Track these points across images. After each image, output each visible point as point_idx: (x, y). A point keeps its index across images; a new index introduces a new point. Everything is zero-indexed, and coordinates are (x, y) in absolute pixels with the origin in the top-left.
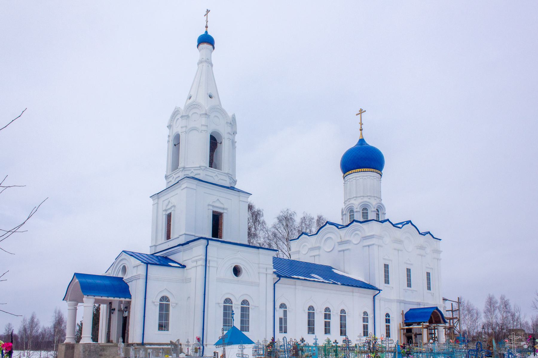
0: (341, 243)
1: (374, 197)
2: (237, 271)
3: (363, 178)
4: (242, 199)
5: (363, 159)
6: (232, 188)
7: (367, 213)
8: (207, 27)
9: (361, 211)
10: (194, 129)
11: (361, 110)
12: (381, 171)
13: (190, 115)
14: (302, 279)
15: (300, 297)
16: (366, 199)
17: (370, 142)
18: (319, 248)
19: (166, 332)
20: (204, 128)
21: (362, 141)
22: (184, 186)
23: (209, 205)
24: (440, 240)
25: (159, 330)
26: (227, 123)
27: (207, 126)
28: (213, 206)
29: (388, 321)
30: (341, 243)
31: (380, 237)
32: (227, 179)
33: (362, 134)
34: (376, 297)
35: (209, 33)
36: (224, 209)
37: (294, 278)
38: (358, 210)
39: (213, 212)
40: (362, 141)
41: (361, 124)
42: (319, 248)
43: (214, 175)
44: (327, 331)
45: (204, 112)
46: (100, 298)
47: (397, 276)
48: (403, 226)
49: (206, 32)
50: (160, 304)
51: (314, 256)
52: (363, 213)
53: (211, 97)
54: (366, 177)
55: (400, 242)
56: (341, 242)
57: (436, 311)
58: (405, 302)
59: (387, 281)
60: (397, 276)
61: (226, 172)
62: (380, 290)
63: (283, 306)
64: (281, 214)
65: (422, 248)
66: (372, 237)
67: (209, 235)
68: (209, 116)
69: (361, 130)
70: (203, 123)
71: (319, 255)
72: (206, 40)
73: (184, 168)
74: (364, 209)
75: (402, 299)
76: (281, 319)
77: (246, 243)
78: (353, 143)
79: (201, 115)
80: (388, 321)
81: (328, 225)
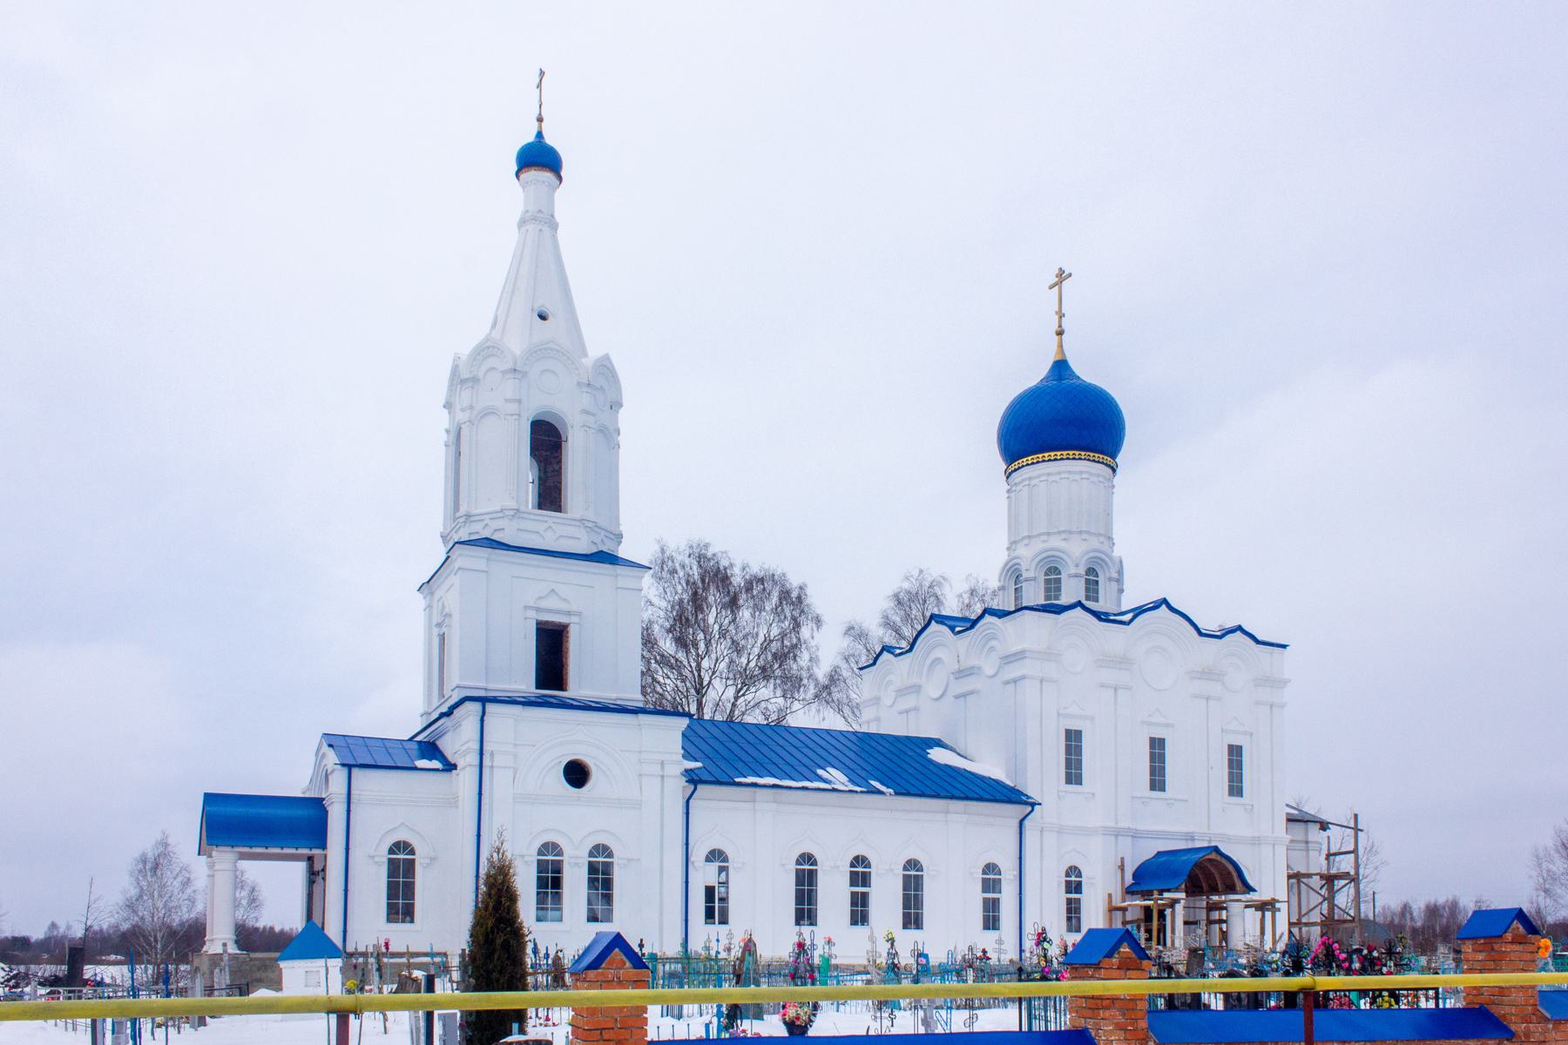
0: (961, 674)
1: (1081, 532)
2: (577, 774)
3: (1062, 477)
4: (622, 582)
5: (1064, 422)
6: (605, 558)
7: (1058, 581)
8: (540, 120)
9: (1042, 578)
10: (489, 412)
11: (1061, 271)
12: (1113, 456)
13: (481, 375)
14: (764, 786)
15: (764, 833)
16: (1055, 542)
17: (1086, 371)
18: (916, 689)
19: (407, 926)
20: (513, 408)
21: (1061, 367)
22: (457, 565)
23: (526, 608)
24: (1284, 646)
25: (389, 920)
26: (579, 384)
27: (519, 401)
28: (538, 610)
29: (1074, 887)
30: (961, 674)
31: (1048, 655)
32: (581, 533)
33: (1061, 346)
34: (1026, 822)
35: (549, 140)
36: (569, 613)
37: (740, 784)
38: (1031, 574)
39: (539, 623)
40: (1061, 367)
41: (1061, 316)
42: (916, 689)
43: (541, 527)
44: (859, 912)
45: (509, 365)
46: (246, 850)
47: (1114, 761)
48: (1134, 617)
49: (540, 135)
50: (390, 860)
51: (907, 711)
52: (1047, 582)
53: (543, 317)
54: (1057, 478)
55: (1123, 662)
56: (960, 671)
57: (1213, 856)
58: (1136, 835)
59: (1073, 775)
60: (1114, 761)
61: (578, 516)
62: (1033, 805)
63: (716, 855)
64: (906, 585)
65: (1207, 674)
66: (1019, 656)
67: (525, 683)
68: (525, 374)
69: (1060, 333)
70: (510, 395)
71: (916, 709)
72: (539, 158)
73: (468, 516)
74: (1050, 571)
75: (1123, 824)
76: (710, 891)
77: (634, 696)
78: (1034, 374)
79: (504, 372)
80: (1074, 887)
81: (988, 619)
